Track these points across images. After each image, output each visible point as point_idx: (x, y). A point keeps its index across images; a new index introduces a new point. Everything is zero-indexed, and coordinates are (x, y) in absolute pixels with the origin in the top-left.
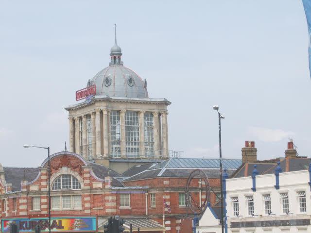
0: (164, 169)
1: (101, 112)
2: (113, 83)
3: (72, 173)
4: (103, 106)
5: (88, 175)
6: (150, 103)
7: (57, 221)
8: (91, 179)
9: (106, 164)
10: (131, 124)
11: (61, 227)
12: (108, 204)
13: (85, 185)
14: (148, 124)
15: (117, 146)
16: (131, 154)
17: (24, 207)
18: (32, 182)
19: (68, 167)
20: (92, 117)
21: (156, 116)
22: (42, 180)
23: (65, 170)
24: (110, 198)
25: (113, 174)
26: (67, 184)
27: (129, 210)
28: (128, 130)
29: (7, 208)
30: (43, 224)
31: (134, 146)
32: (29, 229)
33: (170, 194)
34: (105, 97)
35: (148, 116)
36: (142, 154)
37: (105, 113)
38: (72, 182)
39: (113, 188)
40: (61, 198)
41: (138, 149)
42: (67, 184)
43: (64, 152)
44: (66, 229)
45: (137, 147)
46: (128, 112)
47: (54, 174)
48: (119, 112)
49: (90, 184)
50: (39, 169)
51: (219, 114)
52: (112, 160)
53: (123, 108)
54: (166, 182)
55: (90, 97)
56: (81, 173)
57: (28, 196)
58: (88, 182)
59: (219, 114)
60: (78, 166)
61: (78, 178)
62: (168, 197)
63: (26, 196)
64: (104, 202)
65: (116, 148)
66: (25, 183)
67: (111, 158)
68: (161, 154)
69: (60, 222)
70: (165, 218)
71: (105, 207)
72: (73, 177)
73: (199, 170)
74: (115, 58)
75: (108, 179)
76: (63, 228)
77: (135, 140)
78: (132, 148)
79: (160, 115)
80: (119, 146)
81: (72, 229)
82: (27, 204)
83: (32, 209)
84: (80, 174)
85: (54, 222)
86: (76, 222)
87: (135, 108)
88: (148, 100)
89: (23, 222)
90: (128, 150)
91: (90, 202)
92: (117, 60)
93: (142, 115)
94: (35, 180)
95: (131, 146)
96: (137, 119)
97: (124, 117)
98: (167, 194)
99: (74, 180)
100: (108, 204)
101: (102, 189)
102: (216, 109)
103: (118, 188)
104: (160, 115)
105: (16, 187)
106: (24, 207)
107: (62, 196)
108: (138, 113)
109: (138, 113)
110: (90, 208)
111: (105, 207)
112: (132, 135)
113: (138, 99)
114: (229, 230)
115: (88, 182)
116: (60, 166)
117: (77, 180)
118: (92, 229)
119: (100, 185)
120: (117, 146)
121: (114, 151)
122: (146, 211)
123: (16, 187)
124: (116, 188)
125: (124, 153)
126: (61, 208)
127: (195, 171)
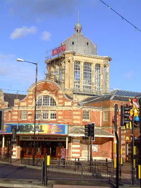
3: (51, 95)
11: (41, 131)
15: (78, 84)
18: (22, 100)
19: (48, 91)
22: (28, 99)
23: (45, 93)
26: (46, 102)
28: (85, 74)
30: (29, 127)
35: (97, 66)
38: (50, 101)
42: (46, 102)
48: (79, 62)
49: (63, 103)
56: (56, 94)
57: (19, 110)
58: (61, 101)
60: (54, 90)
61: (54, 98)
63: (17, 109)
65: (77, 85)
72: (51, 97)
76: (43, 131)
84: (56, 95)
86: (53, 127)
88: (42, 170)
93: (94, 65)
99: (51, 100)
100: (75, 117)
105: (11, 105)
106: (16, 117)
112: (87, 74)
113: (42, 179)
115: (61, 101)
117: (54, 100)
118: (64, 133)
120: (78, 84)
122: (100, 124)
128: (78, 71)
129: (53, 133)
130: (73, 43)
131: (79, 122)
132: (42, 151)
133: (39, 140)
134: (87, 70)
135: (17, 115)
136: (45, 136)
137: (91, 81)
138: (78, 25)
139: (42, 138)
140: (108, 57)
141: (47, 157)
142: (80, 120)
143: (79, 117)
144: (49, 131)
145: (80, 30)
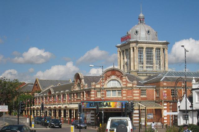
0: (164, 77)
1: (133, 48)
2: (139, 33)
4: (134, 45)
5: (125, 80)
6: (147, 43)
7: (108, 103)
8: (127, 82)
9: (135, 74)
10: (149, 54)
12: (134, 95)
13: (123, 85)
14: (158, 54)
16: (148, 69)
17: (93, 96)
18: (97, 83)
20: (129, 50)
21: (162, 50)
24: (136, 92)
25: (138, 80)
27: (146, 98)
29: (85, 96)
31: (150, 65)
32: (94, 107)
33: (126, 90)
34: (135, 40)
36: (155, 69)
37: (135, 48)
39: (137, 87)
40: (117, 92)
41: (152, 67)
43: (113, 68)
44: (112, 107)
45: (152, 65)
46: (147, 48)
47: (108, 79)
48: (142, 48)
50: (101, 77)
51: (185, 49)
52: (139, 72)
53: (144, 46)
54: (165, 84)
55: (127, 40)
58: (124, 83)
59: (185, 49)
62: (165, 91)
64: (132, 93)
66: (94, 83)
67: (138, 71)
68: (164, 69)
69: (110, 103)
70: (164, 102)
71: (133, 96)
73: (182, 78)
74: (141, 20)
75: (135, 82)
76: (111, 106)
77: (151, 62)
78: (149, 66)
79: (164, 49)
80: (142, 65)
81: (115, 107)
82: (139, 93)
83: (97, 96)
84: (121, 79)
85: (107, 103)
87: (151, 46)
89: (92, 103)
90: (147, 67)
91: (94, 94)
92: (142, 21)
93: (154, 49)
94: (98, 82)
95: (149, 65)
96: (152, 52)
97: (145, 51)
98: (165, 90)
100: (134, 95)
101: (132, 87)
102: (183, 46)
103: (140, 87)
104: (164, 49)
106: (93, 96)
107: (112, 91)
108: (152, 48)
109: (152, 48)
110: (94, 97)
111: (133, 96)
114: (196, 106)
115: (124, 83)
116: (111, 75)
119: (131, 85)
121: (140, 68)
123: (90, 85)
124: (139, 86)
125: (145, 69)
126: (112, 96)
127: (179, 78)
128: (141, 54)
129: (118, 107)
130: (137, 32)
131: (138, 98)
132: (5, 86)
133: (110, 111)
134: (149, 52)
135: (94, 94)
136: (111, 110)
137: (152, 62)
138: (141, 15)
139: (115, 110)
140: (165, 41)
141: (77, 104)
142: (139, 96)
143: (138, 95)
144: (116, 106)
145: (143, 20)
